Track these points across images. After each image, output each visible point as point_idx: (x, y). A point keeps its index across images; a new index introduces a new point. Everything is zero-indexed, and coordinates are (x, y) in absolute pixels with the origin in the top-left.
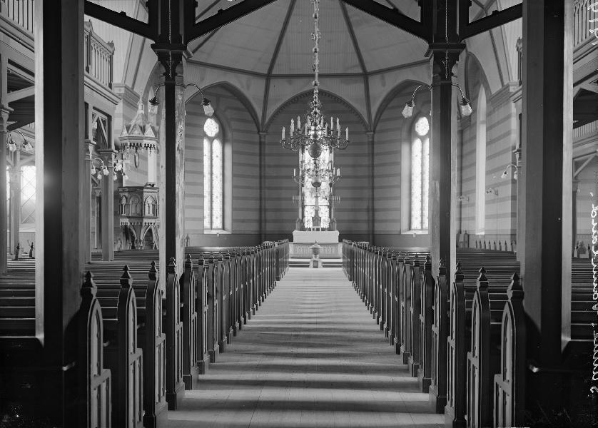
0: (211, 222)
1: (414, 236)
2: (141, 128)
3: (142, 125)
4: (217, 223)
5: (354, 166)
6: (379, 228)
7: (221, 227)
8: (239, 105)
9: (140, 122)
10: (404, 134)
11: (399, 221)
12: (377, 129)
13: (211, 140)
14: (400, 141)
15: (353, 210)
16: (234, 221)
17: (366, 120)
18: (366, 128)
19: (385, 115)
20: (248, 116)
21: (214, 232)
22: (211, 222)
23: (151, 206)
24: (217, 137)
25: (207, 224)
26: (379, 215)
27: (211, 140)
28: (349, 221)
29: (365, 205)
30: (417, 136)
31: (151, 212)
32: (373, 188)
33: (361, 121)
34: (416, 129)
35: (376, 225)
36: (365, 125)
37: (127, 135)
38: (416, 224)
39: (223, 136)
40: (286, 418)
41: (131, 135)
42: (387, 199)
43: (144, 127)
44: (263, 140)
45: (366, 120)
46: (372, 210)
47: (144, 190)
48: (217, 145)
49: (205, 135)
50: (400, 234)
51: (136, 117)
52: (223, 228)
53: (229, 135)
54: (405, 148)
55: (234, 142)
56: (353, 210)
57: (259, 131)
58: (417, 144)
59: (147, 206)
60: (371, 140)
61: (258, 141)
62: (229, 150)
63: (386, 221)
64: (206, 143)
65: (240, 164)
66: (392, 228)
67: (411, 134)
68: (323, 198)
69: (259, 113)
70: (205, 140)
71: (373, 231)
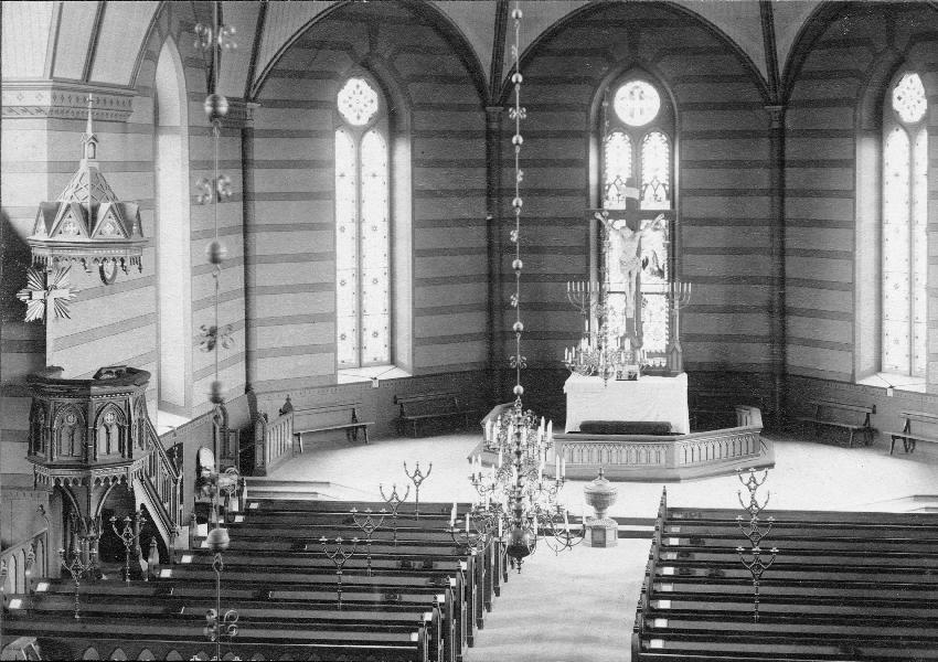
0: (360, 348)
1: (890, 393)
2: (84, 212)
3: (88, 204)
4: (377, 348)
5: (733, 193)
6: (797, 358)
7: (386, 357)
8: (433, 39)
9: (84, 197)
10: (865, 113)
11: (850, 347)
12: (793, 97)
13: (359, 134)
14: (850, 135)
15: (729, 309)
16: (418, 341)
17: (764, 74)
18: (764, 93)
19: (814, 62)
20: (453, 64)
21: (365, 375)
22: (360, 348)
23: (115, 431)
24: (374, 123)
25: (346, 352)
26: (798, 327)
27: (359, 134)
28: (719, 338)
29: (762, 293)
30: (897, 121)
31: (115, 447)
32: (783, 253)
33: (751, 73)
34: (896, 105)
35: (790, 349)
36: (759, 83)
37: (45, 237)
38: (895, 356)
39: (390, 121)
40: (822, 87)
41: (58, 238)
42: (819, 285)
43: (95, 209)
44: (494, 126)
45: (764, 74)
46: (780, 311)
47: (94, 389)
48: (375, 143)
49: (340, 122)
50: (852, 383)
51: (77, 181)
52: (393, 361)
53: (405, 119)
54: (866, 153)
55: (417, 136)
56: (729, 309)
57: (484, 106)
58: (896, 140)
59: (102, 432)
60: (776, 125)
61: (483, 128)
62: (404, 153)
63: (815, 343)
64: (342, 140)
65: (431, 194)
66: (831, 365)
67: (880, 120)
68: (653, 273)
69: (484, 56)
70: (339, 134)
71: (784, 364)
